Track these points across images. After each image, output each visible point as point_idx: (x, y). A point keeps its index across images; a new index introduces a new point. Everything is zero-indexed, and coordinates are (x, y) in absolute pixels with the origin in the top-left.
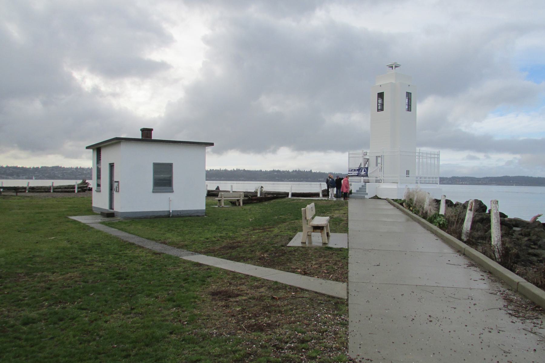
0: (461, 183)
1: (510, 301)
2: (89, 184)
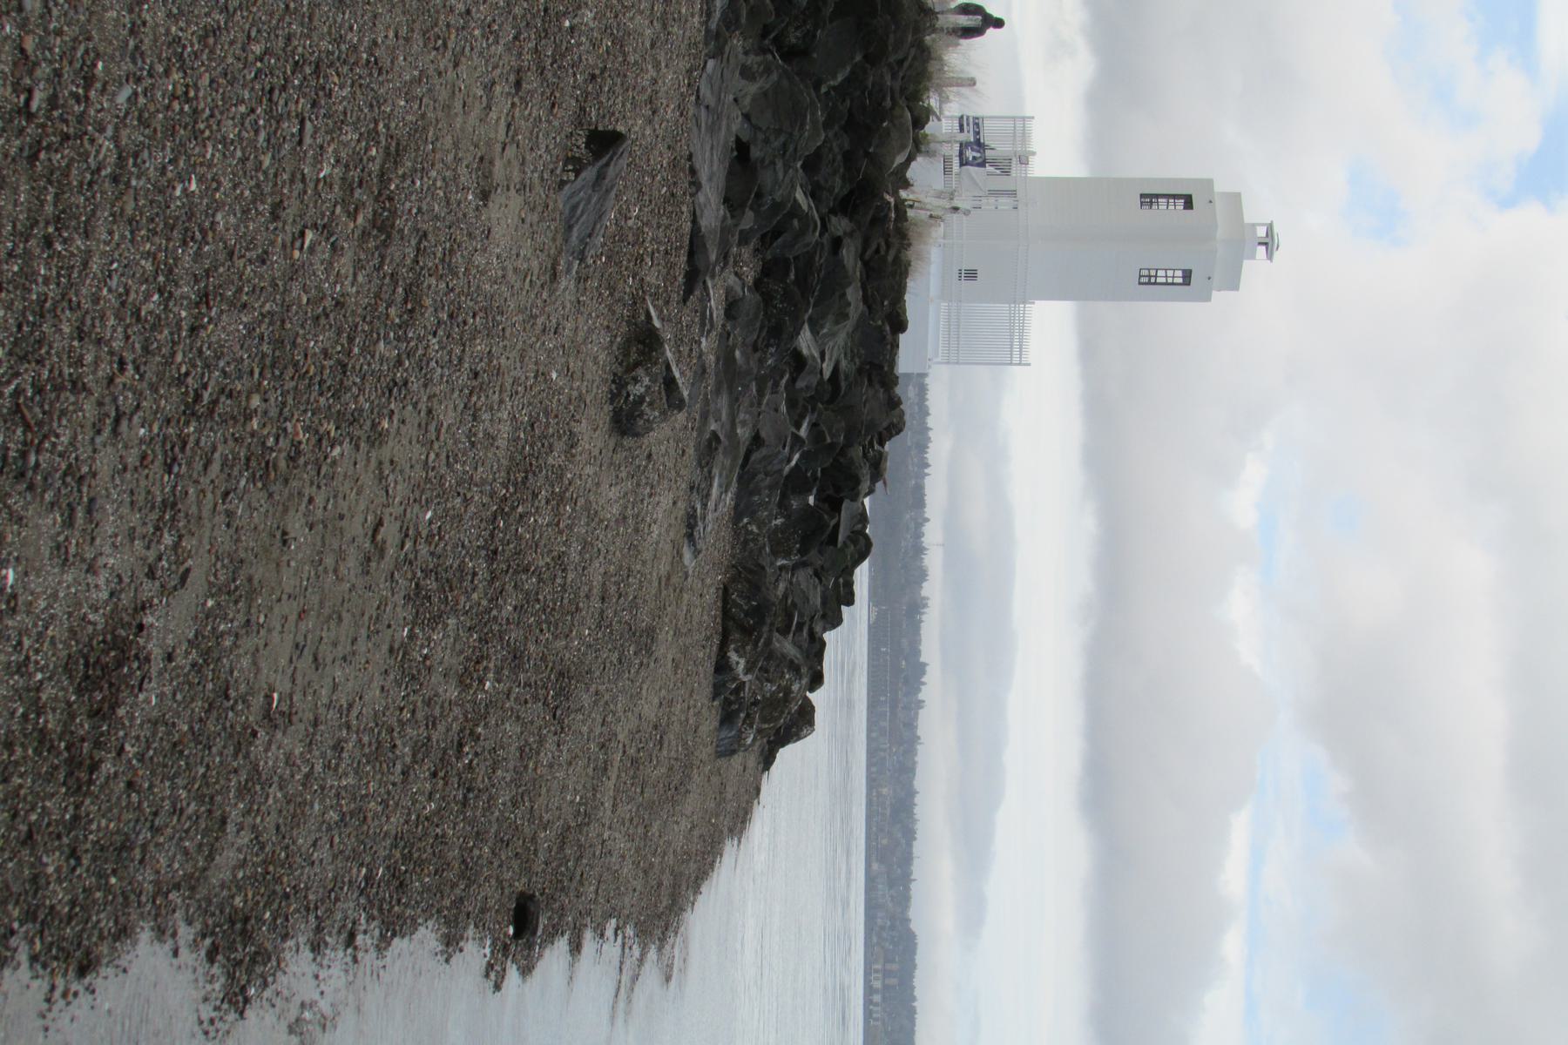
0: (877, 984)
1: (381, 443)
2: (513, 974)
